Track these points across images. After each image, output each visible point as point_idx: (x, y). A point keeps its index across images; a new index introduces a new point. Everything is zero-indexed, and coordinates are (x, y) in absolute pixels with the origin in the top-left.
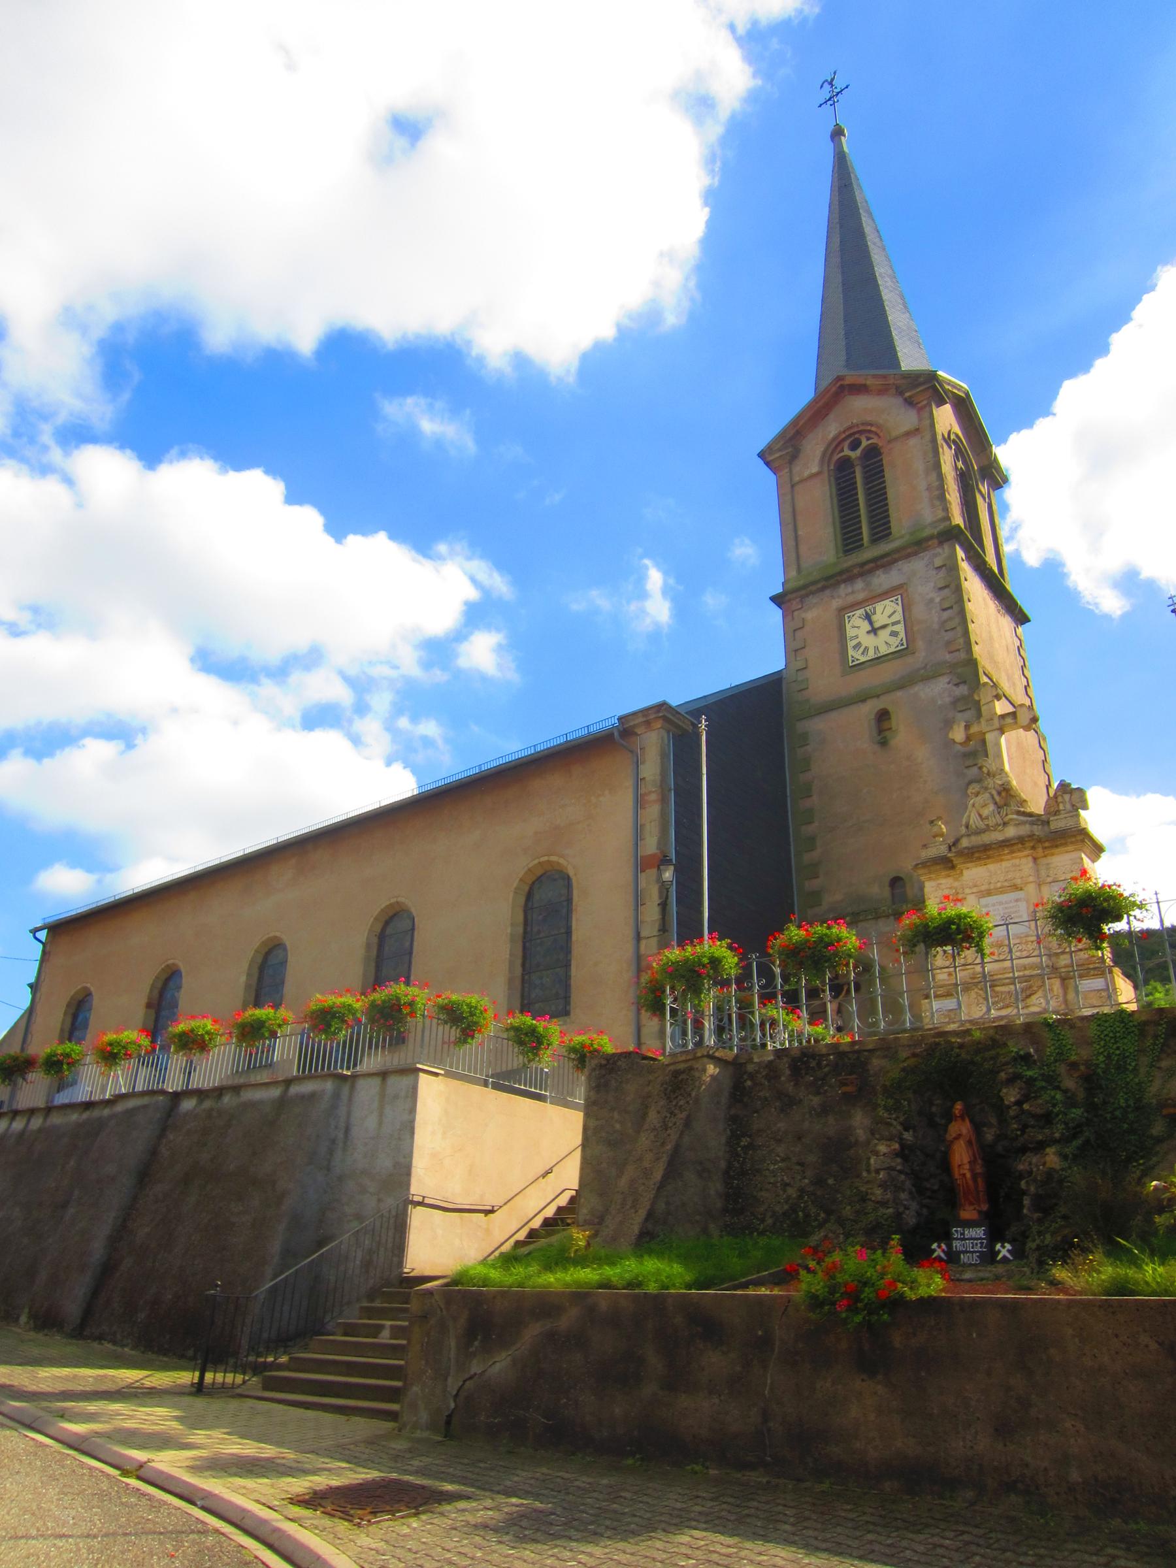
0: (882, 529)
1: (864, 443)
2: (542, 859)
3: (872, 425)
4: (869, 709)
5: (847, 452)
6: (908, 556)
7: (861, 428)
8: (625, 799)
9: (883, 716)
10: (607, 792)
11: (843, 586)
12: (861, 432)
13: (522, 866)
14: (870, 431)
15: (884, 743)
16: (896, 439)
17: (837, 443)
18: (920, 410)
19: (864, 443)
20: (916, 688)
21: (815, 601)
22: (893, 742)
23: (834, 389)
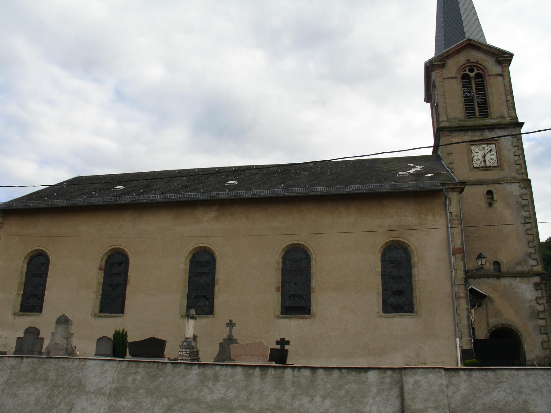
0: (485, 113)
1: (476, 71)
2: (394, 239)
3: (481, 65)
4: (485, 188)
5: (468, 72)
6: (500, 128)
7: (475, 64)
8: (441, 222)
9: (490, 193)
10: (430, 214)
11: (470, 132)
12: (475, 66)
13: (382, 240)
14: (479, 67)
15: (490, 204)
16: (492, 75)
17: (464, 67)
18: (502, 67)
19: (476, 71)
20: (505, 185)
21: (456, 134)
22: (495, 205)
23: (466, 43)
